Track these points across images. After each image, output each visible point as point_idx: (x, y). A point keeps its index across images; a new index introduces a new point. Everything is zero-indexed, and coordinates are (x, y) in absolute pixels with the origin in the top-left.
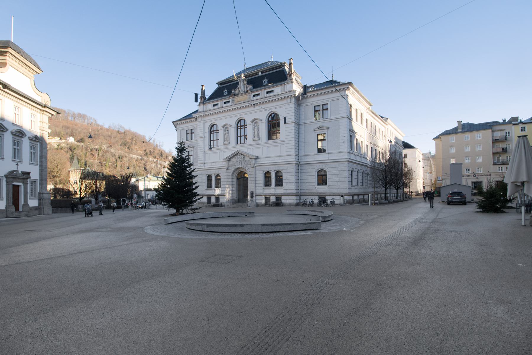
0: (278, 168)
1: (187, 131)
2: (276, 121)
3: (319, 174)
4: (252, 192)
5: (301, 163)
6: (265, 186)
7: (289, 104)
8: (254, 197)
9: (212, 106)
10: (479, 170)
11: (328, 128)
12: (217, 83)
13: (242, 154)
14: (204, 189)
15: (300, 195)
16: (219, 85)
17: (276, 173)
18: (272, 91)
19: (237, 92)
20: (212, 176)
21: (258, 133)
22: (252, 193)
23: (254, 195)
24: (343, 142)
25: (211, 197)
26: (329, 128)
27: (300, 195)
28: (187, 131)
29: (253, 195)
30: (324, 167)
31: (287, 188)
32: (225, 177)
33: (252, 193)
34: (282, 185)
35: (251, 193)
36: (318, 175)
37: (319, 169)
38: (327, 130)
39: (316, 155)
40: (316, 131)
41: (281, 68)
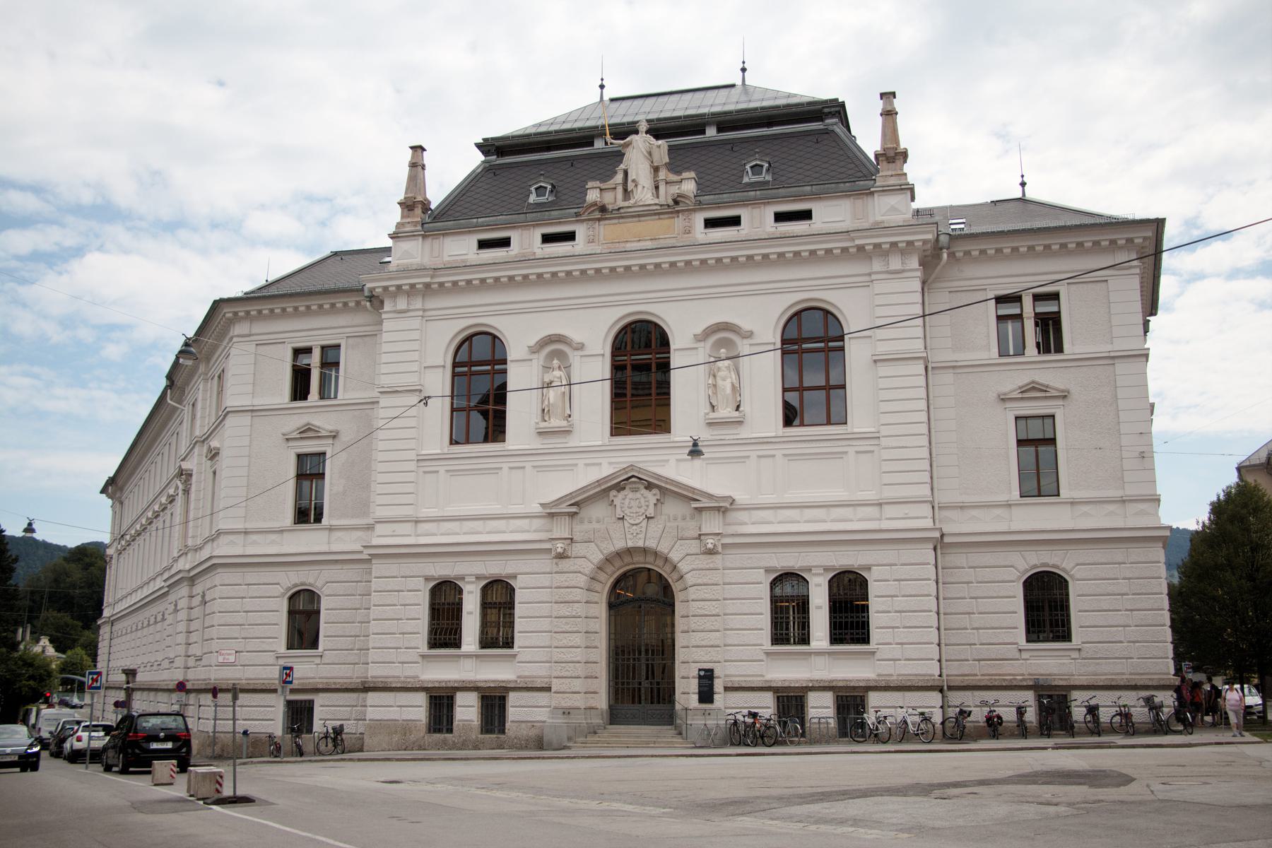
0: (495, 568)
1: (297, 352)
2: (489, 365)
3: (778, 591)
4: (706, 670)
5: (946, 540)
6: (433, 644)
7: (892, 276)
8: (716, 697)
9: (475, 245)
10: (1036, 602)
11: (1064, 396)
12: (479, 146)
13: (649, 486)
14: (413, 655)
15: (945, 688)
16: (486, 153)
17: (485, 590)
18: (806, 215)
19: (613, 199)
20: (461, 591)
21: (736, 389)
22: (706, 680)
23: (718, 685)
24: (1137, 454)
25: (451, 699)
26: (338, 432)
27: (945, 688)
28: (297, 352)
29: (711, 686)
30: (311, 581)
31: (896, 651)
32: (543, 595)
33: (706, 680)
34: (509, 644)
35: (700, 677)
36: (292, 613)
37: (302, 584)
38: (330, 441)
39: (285, 534)
40: (291, 444)
41: (821, 120)
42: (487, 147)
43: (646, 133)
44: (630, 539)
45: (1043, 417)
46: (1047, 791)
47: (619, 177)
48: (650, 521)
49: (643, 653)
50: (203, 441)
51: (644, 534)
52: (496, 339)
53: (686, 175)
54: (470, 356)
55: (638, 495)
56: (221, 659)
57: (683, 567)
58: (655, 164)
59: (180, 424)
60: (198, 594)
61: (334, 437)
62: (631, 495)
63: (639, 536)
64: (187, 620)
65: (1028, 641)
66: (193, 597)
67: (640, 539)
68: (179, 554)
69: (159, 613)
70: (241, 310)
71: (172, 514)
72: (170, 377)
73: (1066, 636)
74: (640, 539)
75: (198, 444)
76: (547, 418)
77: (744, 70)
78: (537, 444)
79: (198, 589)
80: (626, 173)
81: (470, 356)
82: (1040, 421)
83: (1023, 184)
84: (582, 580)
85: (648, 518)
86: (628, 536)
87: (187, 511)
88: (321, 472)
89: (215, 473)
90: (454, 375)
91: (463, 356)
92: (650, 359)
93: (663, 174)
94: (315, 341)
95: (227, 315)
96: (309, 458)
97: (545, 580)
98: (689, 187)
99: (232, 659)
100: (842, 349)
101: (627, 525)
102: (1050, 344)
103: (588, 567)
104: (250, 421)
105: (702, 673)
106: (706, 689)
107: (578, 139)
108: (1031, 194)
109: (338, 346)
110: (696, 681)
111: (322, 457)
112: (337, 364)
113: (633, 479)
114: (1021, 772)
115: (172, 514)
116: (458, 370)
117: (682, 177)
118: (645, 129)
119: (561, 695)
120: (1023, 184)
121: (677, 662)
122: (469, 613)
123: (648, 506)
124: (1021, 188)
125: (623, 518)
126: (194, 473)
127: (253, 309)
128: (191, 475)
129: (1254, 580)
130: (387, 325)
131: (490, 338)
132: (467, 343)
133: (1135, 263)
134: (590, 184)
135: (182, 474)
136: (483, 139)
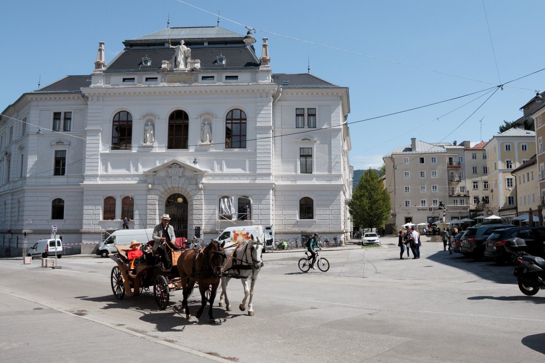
13: (180, 167)
16: (126, 45)
33: (198, 230)
42: (129, 44)
43: (184, 44)
45: (309, 148)
46: (284, 262)
47: (174, 58)
48: (181, 178)
49: (177, 222)
50: (16, 143)
53: (196, 61)
54: (119, 119)
55: (177, 169)
56: (27, 222)
58: (186, 56)
61: (69, 145)
65: (300, 219)
66: (13, 199)
70: (34, 97)
75: (14, 144)
76: (146, 142)
79: (16, 197)
81: (119, 119)
82: (308, 149)
85: (180, 177)
86: (173, 183)
87: (9, 168)
89: (22, 155)
90: (113, 125)
91: (117, 119)
92: (181, 123)
93: (189, 60)
95: (29, 99)
98: (198, 66)
99: (31, 222)
100: (246, 123)
105: (196, 228)
106: (198, 233)
107: (161, 43)
108: (311, 73)
109: (71, 112)
110: (195, 231)
112: (70, 119)
113: (175, 164)
114: (289, 257)
116: (115, 123)
117: (195, 61)
118: (183, 43)
125: (171, 177)
126: (12, 154)
127: (39, 97)
128: (11, 154)
129: (370, 199)
130: (89, 107)
132: (118, 114)
133: (257, 138)
134: (163, 61)
136: (124, 50)
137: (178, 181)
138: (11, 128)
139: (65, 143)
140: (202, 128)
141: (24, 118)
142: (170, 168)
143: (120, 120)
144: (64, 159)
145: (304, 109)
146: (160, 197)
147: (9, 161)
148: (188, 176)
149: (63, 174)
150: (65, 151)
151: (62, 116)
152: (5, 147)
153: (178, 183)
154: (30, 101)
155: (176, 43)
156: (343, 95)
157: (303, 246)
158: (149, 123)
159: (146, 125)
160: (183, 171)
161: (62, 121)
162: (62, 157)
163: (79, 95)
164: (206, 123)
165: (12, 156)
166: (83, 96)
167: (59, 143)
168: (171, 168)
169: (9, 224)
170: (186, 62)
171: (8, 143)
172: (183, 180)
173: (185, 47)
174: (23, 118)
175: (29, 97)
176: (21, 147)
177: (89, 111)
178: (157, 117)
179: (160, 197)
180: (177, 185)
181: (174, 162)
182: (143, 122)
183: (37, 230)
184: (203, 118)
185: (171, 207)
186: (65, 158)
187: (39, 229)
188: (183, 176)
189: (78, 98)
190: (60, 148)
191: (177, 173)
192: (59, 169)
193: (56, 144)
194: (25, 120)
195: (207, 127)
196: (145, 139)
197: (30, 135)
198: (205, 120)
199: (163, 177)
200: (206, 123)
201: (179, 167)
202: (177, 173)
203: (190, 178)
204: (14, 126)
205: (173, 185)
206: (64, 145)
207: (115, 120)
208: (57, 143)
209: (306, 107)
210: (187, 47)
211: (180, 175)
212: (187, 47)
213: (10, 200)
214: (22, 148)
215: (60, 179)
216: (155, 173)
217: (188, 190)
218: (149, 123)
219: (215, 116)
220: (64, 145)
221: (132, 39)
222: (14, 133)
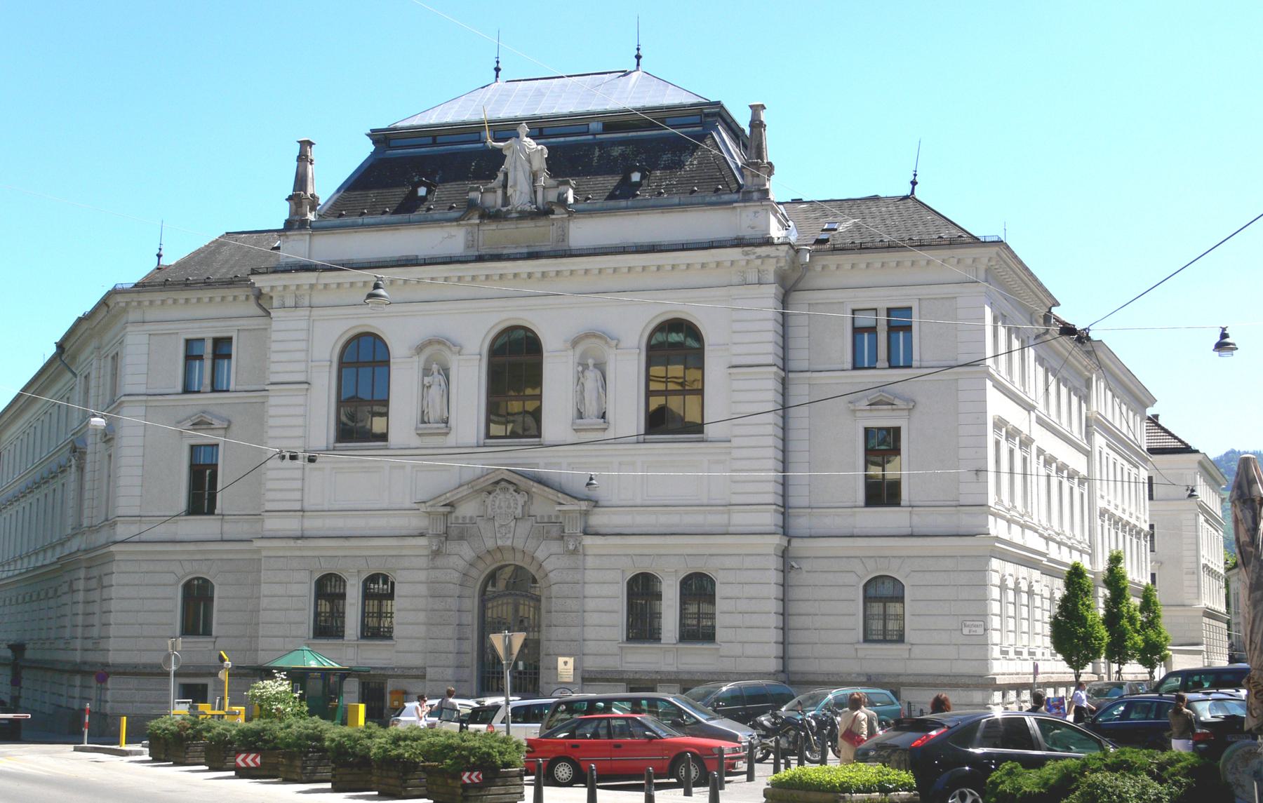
19: (494, 200)
42: (381, 138)
44: (500, 538)
51: (512, 534)
52: (377, 341)
55: (508, 496)
57: (548, 566)
59: (71, 390)
60: (95, 577)
62: (501, 496)
63: (508, 535)
64: (110, 624)
67: (509, 538)
68: (74, 533)
69: (51, 588)
71: (63, 485)
72: (60, 346)
73: (658, 640)
74: (509, 538)
77: (638, 57)
78: (416, 442)
80: (506, 175)
83: (914, 183)
84: (455, 576)
86: (498, 535)
88: (214, 462)
89: (110, 456)
94: (209, 332)
96: (202, 448)
97: (422, 576)
101: (496, 524)
102: (203, 623)
103: (461, 564)
104: (144, 412)
111: (215, 448)
112: (229, 356)
115: (63, 485)
119: (434, 683)
120: (914, 183)
121: (541, 654)
122: (351, 604)
123: (516, 508)
124: (911, 186)
131: (371, 339)
135: (75, 452)
137: (512, 530)
138: (113, 358)
139: (217, 423)
140: (579, 379)
141: (114, 353)
142: (490, 493)
143: (355, 370)
144: (214, 468)
145: (876, 309)
146: (457, 681)
147: (81, 469)
148: (542, 517)
149: (211, 512)
150: (217, 445)
151: (208, 349)
152: (27, 469)
153: (511, 535)
154: (125, 310)
155: (506, 129)
156: (993, 263)
157: (536, 171)
158: (435, 367)
159: (427, 372)
160: (525, 502)
161: (208, 364)
162: (208, 462)
163: (248, 291)
164: (591, 362)
165: (89, 458)
166: (259, 295)
167: (200, 424)
168: (494, 494)
169: (79, 648)
170: (534, 186)
171: (81, 417)
172: (524, 528)
173: (531, 144)
174: (112, 355)
175: (121, 299)
176: (106, 435)
177: (274, 336)
178: (453, 349)
179: (457, 681)
180: (509, 543)
181: (499, 478)
182: (417, 363)
183: (143, 664)
184: (580, 348)
185: (495, 604)
186: (217, 465)
187: (149, 661)
188: (526, 515)
189: (247, 298)
190: (204, 437)
191: (509, 507)
192: (209, 489)
193: (191, 427)
194: (115, 358)
195: (592, 377)
196: (423, 412)
197: (125, 404)
198: (584, 355)
199: (471, 518)
200: (591, 362)
201: (515, 491)
202: (509, 507)
203: (546, 520)
204: (93, 375)
205: (500, 543)
206: (213, 429)
207: (344, 360)
208: (193, 425)
209: (883, 305)
210: (538, 144)
211: (519, 512)
212: (538, 144)
213: (82, 582)
214: (108, 437)
215: (202, 526)
216: (448, 509)
217: (540, 554)
218: (435, 367)
219: (614, 343)
220: (213, 429)
221: (433, 118)
222: (92, 392)
